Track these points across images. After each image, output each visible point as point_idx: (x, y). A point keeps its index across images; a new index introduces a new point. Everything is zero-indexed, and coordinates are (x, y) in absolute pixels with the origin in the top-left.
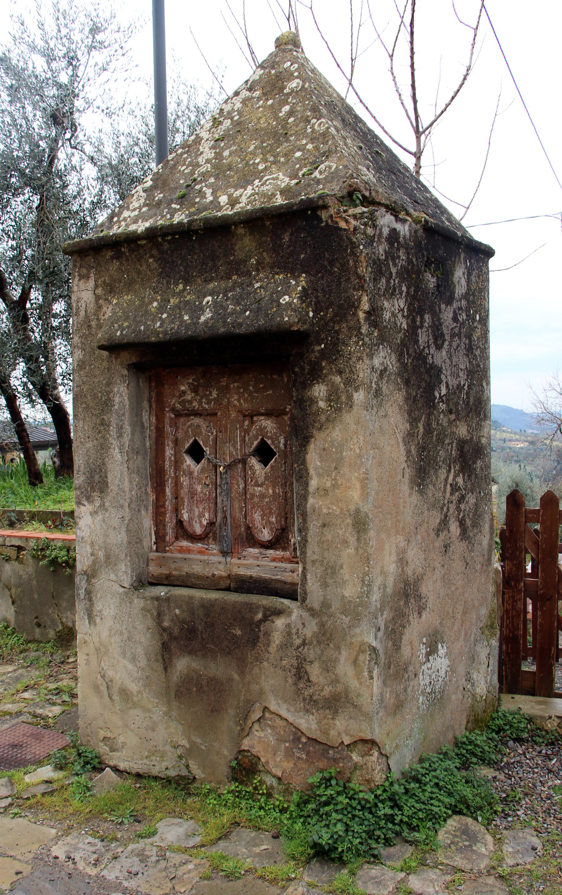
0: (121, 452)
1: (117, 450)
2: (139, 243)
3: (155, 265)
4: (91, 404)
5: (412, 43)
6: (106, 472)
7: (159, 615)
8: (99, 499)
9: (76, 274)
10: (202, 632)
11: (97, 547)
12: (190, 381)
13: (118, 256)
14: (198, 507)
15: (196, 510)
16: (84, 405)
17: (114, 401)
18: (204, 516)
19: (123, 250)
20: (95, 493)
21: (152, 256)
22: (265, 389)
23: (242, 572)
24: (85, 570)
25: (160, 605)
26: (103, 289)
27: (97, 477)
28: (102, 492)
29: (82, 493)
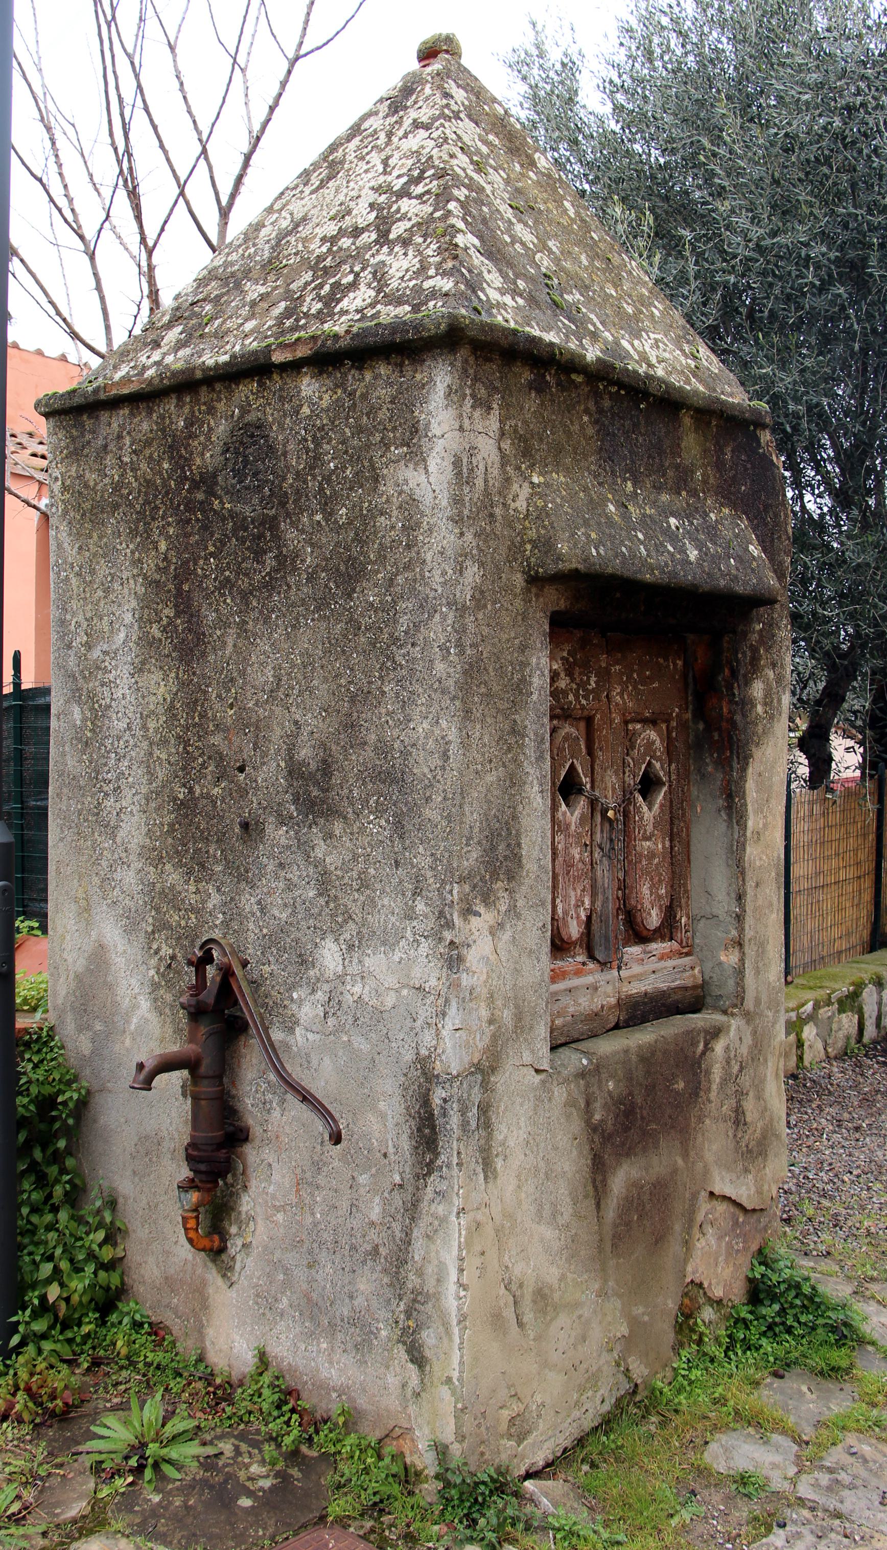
0: (542, 792)
1: (536, 788)
2: (574, 376)
3: (590, 431)
4: (496, 688)
5: (29, 85)
6: (518, 835)
7: (588, 1104)
8: (506, 895)
9: (468, 392)
10: (641, 1108)
11: (499, 1003)
12: (565, 654)
13: (539, 387)
14: (574, 889)
15: (572, 894)
16: (483, 690)
17: (531, 683)
18: (583, 903)
19: (548, 378)
20: (499, 884)
21: (587, 411)
22: (651, 679)
23: (636, 988)
24: (476, 1061)
25: (587, 1086)
26: (513, 444)
27: (502, 847)
28: (511, 878)
29: (475, 887)
